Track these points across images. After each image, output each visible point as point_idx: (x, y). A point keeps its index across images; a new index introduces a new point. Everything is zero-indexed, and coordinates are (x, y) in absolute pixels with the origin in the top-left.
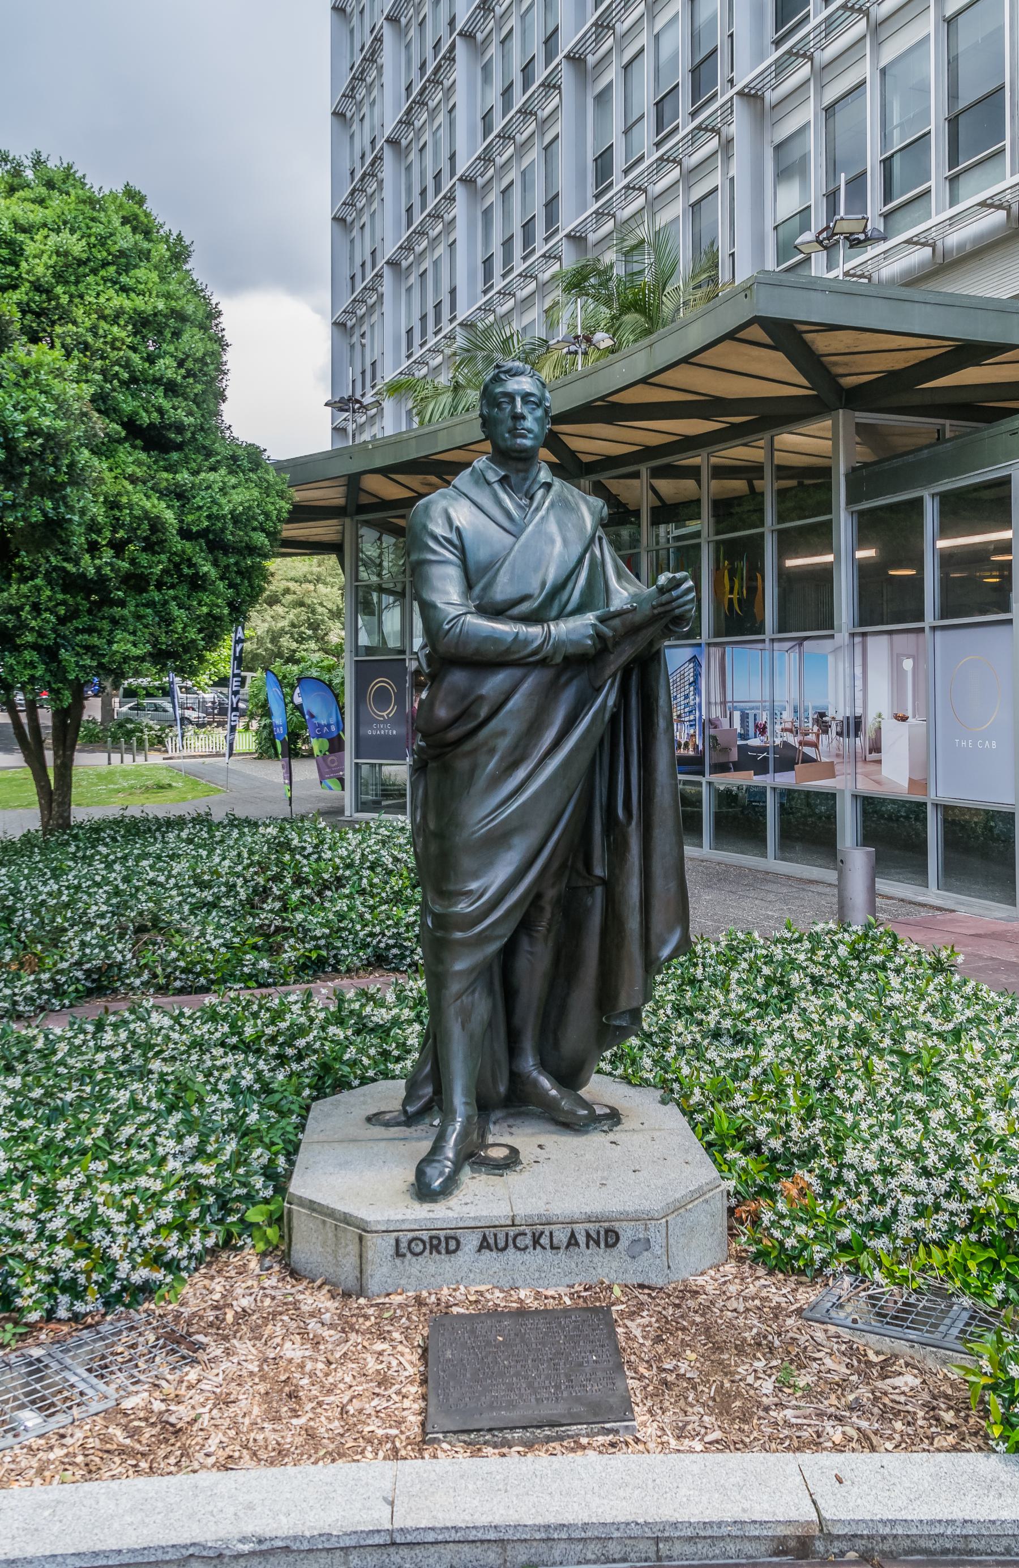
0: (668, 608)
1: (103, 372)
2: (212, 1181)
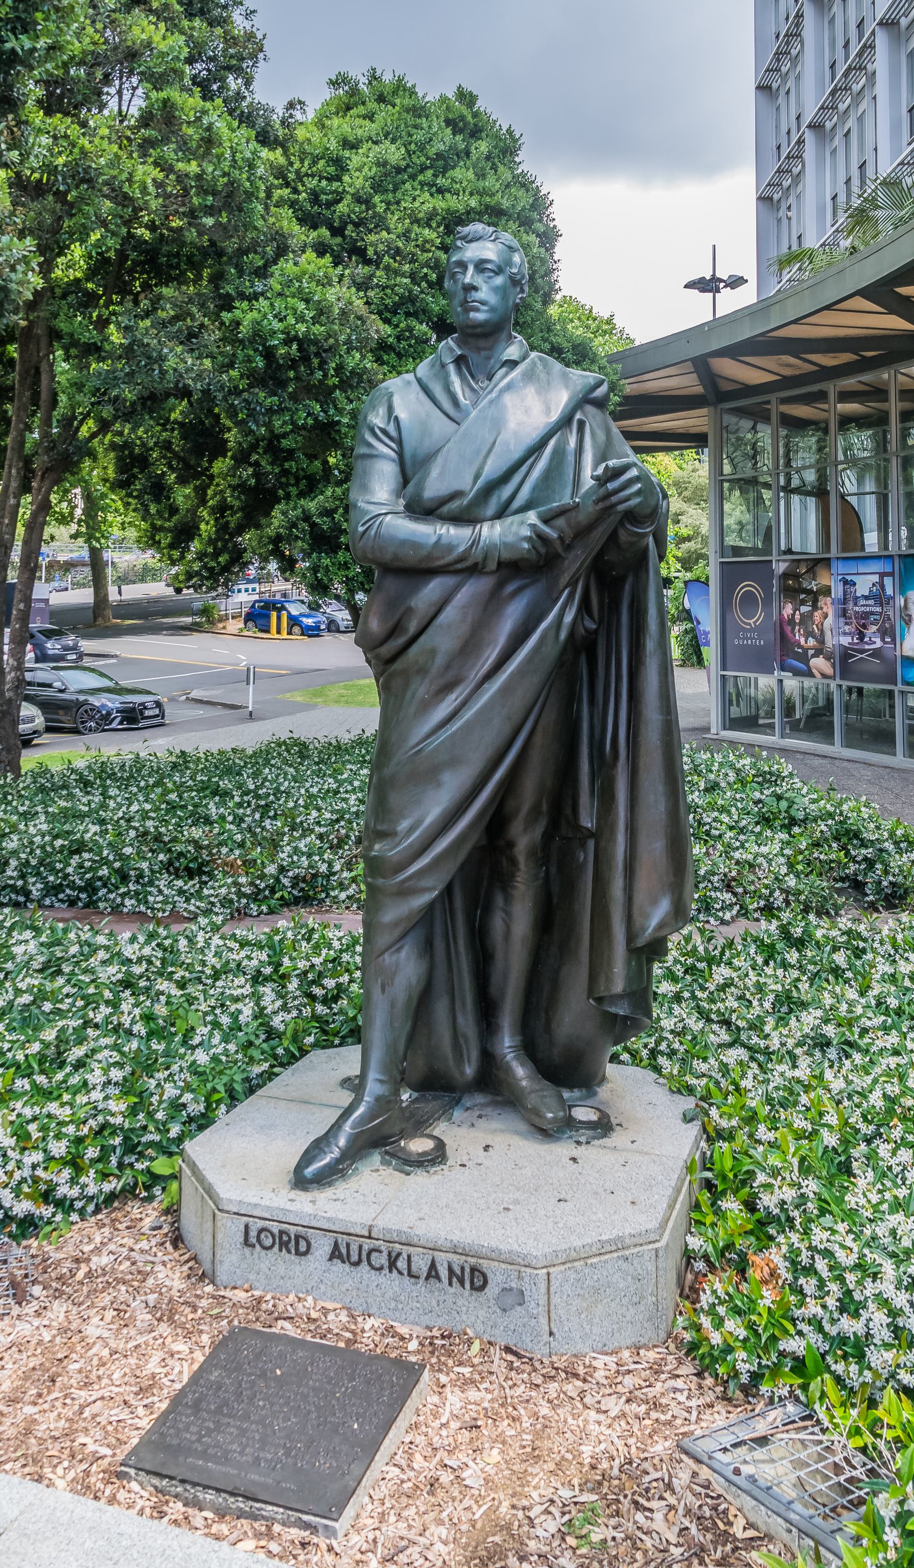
0: (607, 503)
1: (412, 276)
2: (119, 1120)
